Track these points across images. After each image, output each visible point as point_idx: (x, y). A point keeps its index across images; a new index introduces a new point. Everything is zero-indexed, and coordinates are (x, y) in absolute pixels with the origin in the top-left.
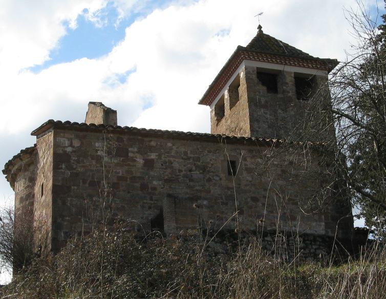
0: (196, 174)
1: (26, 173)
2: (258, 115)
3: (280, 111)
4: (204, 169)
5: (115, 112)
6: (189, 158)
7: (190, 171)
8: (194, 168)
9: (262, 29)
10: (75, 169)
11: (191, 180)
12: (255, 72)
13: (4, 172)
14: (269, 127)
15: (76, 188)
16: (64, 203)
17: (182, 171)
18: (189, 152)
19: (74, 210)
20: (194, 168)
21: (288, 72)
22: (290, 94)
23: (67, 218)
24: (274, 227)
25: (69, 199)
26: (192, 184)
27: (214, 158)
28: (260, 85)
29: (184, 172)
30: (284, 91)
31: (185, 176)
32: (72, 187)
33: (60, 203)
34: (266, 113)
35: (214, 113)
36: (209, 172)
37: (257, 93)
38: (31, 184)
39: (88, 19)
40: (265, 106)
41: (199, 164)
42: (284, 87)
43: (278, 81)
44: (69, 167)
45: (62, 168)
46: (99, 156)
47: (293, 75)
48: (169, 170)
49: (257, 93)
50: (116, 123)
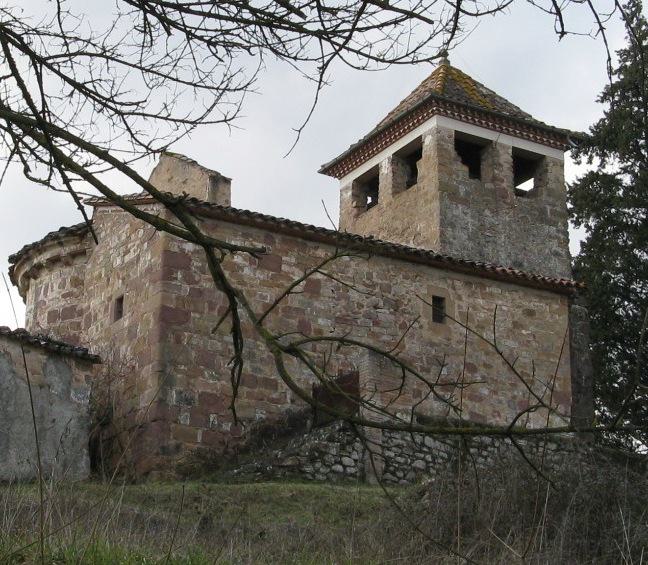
0: (385, 314)
1: (67, 270)
2: (454, 216)
3: (487, 212)
4: (396, 306)
5: (227, 181)
6: (374, 285)
7: (376, 307)
8: (381, 304)
9: (448, 58)
10: (197, 283)
11: (376, 323)
12: (453, 139)
13: (12, 259)
14: (469, 239)
15: (197, 316)
16: (178, 341)
17: (363, 306)
18: (374, 274)
19: (193, 354)
20: (381, 304)
21: (504, 147)
22: (504, 185)
23: (183, 367)
24: (76, 332)
25: (186, 334)
26: (376, 329)
27: (412, 288)
28: (459, 163)
29: (365, 309)
30: (494, 179)
31: (368, 316)
32: (192, 314)
33: (172, 340)
34: (466, 214)
35: (350, 193)
36: (404, 312)
37: (454, 176)
38: (75, 290)
39: (579, 180)
40: (465, 202)
41: (389, 296)
42: (496, 172)
43: (483, 157)
44: (189, 279)
45: (176, 279)
46: (235, 264)
47: (510, 151)
48: (343, 302)
49: (454, 176)
50: (228, 201)
